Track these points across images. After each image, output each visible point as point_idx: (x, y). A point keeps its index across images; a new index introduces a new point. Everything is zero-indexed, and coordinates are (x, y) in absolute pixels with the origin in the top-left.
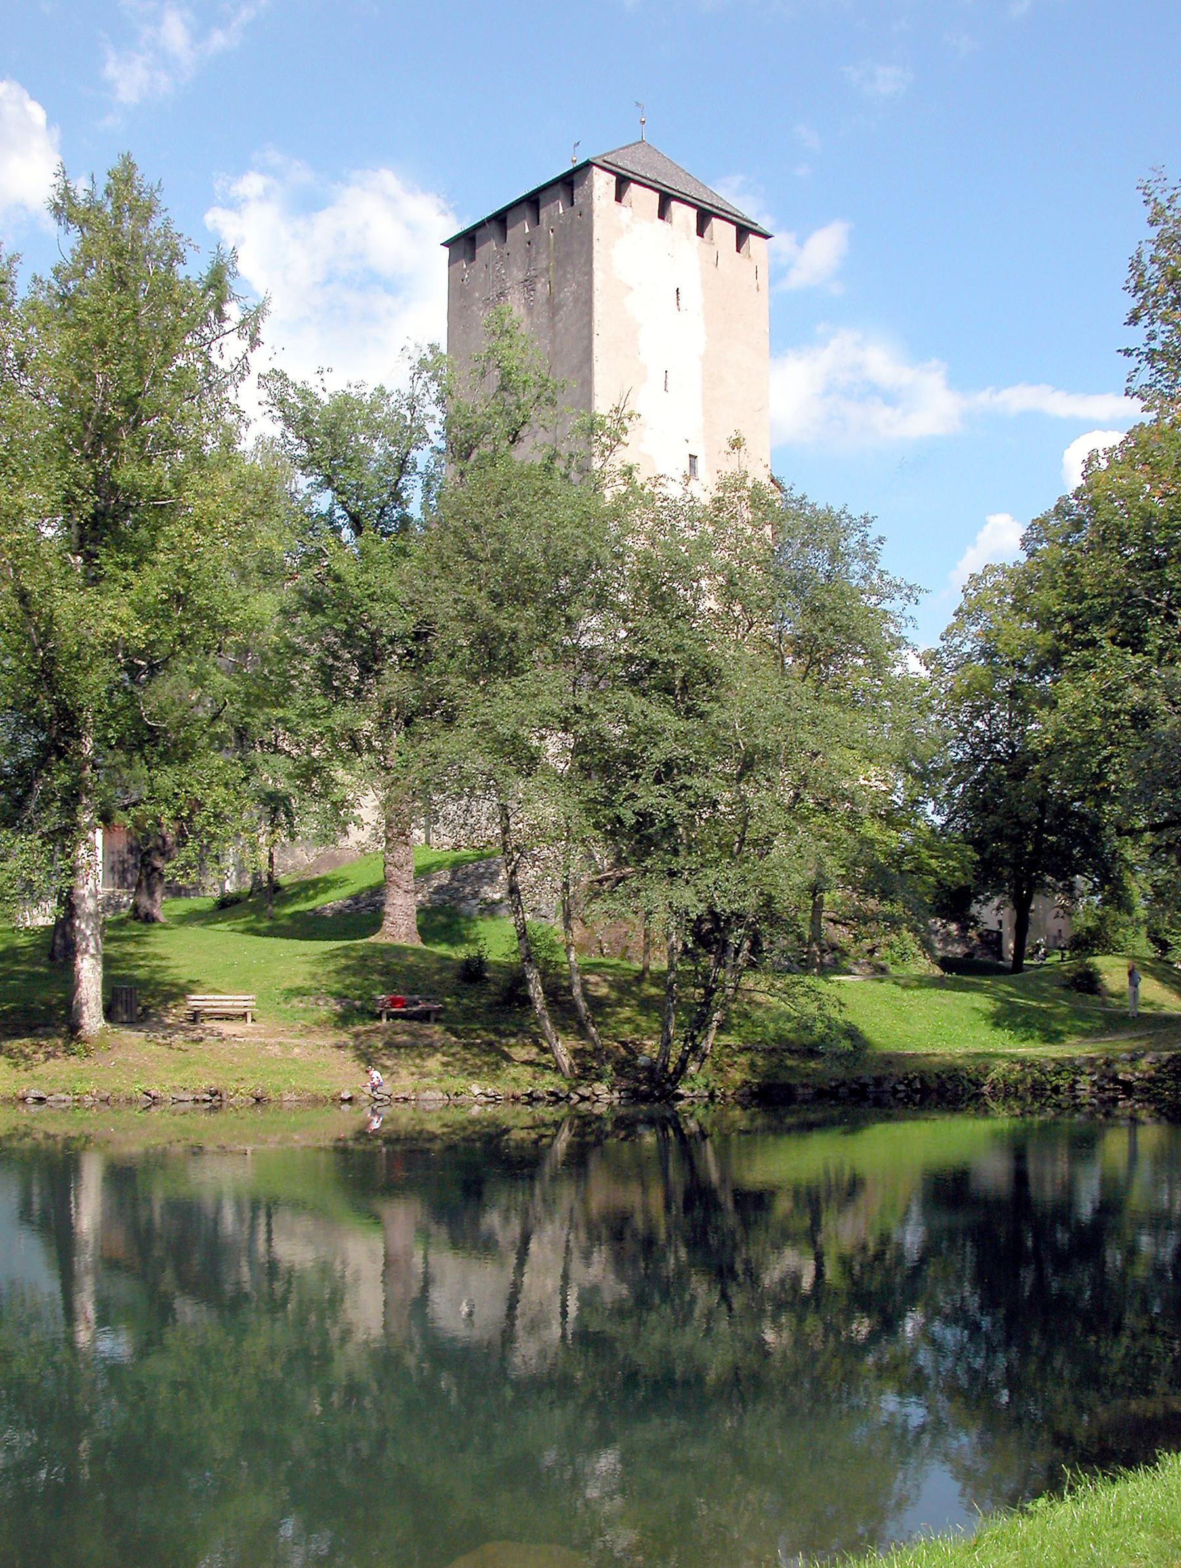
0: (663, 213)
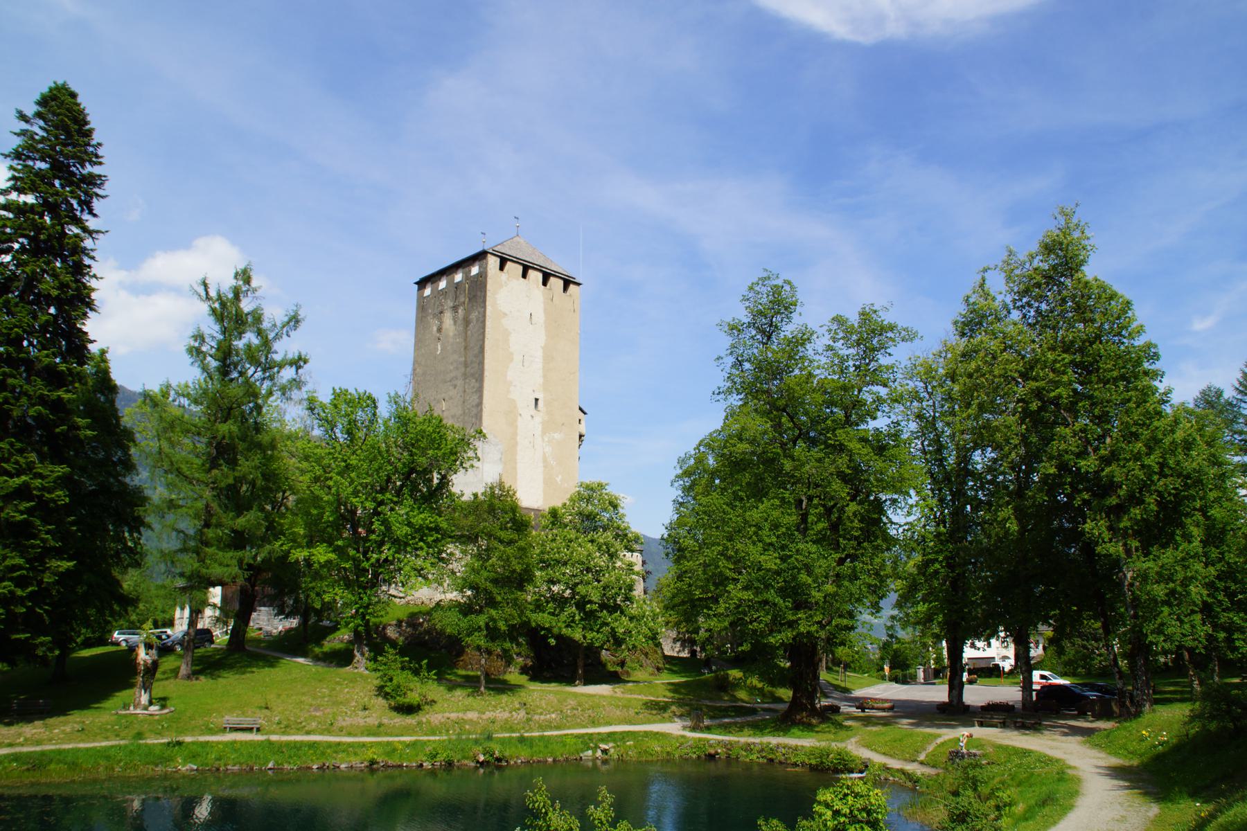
0: (524, 275)
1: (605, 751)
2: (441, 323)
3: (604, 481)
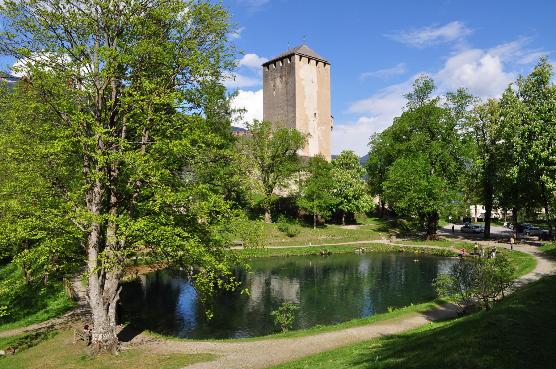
1: (363, 250)
2: (275, 82)
3: (352, 150)
